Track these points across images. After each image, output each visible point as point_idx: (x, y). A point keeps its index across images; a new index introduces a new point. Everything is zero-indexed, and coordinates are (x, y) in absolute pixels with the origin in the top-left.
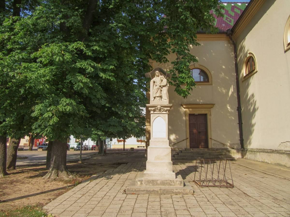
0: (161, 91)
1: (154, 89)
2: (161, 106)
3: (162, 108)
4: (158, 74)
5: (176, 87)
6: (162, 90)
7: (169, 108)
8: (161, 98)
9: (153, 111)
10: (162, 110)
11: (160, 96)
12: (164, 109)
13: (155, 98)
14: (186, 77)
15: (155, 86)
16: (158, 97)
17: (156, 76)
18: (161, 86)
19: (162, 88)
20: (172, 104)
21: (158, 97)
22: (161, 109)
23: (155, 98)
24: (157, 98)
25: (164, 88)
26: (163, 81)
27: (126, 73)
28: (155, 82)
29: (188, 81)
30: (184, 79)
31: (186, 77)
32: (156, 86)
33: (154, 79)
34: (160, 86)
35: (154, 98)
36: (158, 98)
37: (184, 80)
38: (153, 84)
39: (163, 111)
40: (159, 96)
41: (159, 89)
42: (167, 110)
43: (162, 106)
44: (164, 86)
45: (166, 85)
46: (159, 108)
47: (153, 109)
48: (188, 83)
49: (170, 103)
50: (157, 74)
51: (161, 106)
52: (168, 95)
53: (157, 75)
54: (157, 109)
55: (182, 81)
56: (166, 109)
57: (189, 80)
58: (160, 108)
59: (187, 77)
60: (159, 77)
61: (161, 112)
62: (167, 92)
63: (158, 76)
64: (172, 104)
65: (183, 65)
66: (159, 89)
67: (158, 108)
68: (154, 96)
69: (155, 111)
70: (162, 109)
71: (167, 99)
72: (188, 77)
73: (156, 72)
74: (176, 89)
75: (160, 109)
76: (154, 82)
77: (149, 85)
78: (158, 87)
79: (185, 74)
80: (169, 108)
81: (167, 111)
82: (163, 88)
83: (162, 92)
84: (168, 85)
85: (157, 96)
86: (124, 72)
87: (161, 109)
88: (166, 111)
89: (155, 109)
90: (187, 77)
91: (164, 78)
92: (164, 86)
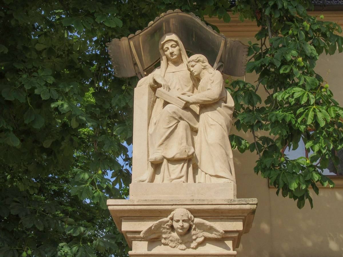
0: (194, 131)
1: (154, 120)
2: (192, 211)
3: (197, 220)
4: (175, 50)
5: (261, 154)
6: (199, 126)
7: (238, 226)
8: (191, 169)
9: (146, 243)
10: (199, 235)
11: (185, 156)
12: (211, 229)
13: (157, 166)
14: (308, 100)
15: (159, 103)
16: (173, 161)
17: (168, 59)
18: (193, 107)
19: (197, 117)
20: (255, 201)
21: (173, 161)
22: (190, 227)
23: (157, 166)
24: (172, 167)
25: (207, 116)
26: (201, 83)
27: (36, 92)
28: (160, 86)
29: (320, 116)
30: (301, 110)
31: (308, 100)
32: (166, 103)
33: (157, 74)
34: (187, 107)
35: (151, 170)
36: (177, 169)
37: (301, 114)
38: (149, 99)
39: (206, 240)
40: (178, 156)
41: (181, 118)
42: (226, 236)
43: (196, 213)
44: (205, 106)
45: (217, 97)
46: (181, 223)
47: (143, 226)
48: (322, 124)
49: (241, 193)
50: (171, 50)
51: (192, 211)
52: (231, 156)
53: (171, 54)
54: (172, 228)
55: (288, 120)
56: (221, 226)
57: (324, 111)
58: (189, 220)
59: (313, 101)
60: (183, 67)
61: (194, 244)
62: (223, 137)
63: (177, 62)
64: (255, 201)
65: (291, 49)
66: (181, 118)
67: (176, 225)
68: (156, 155)
69: (161, 244)
70: (200, 226)
71: (226, 174)
72: (317, 103)
73: (168, 37)
74: (260, 162)
75: (186, 225)
76: (155, 86)
77: (132, 135)
78: (175, 107)
79: (303, 87)
80: (238, 226)
81: (229, 243)
82: (202, 116)
83: (197, 138)
84: (231, 102)
85: (170, 155)
86: (27, 87)
87: (190, 227)
88: (219, 241)
89: (158, 227)
90: (313, 101)
91: (207, 63)
92: (205, 106)
